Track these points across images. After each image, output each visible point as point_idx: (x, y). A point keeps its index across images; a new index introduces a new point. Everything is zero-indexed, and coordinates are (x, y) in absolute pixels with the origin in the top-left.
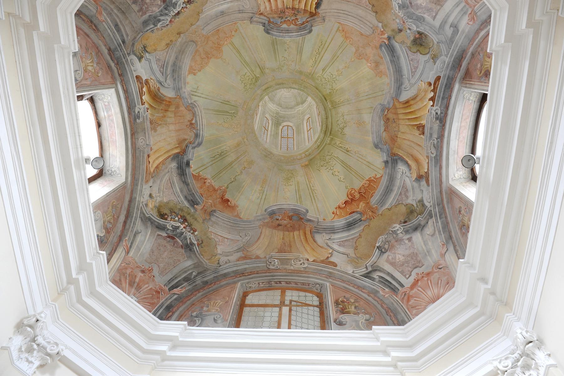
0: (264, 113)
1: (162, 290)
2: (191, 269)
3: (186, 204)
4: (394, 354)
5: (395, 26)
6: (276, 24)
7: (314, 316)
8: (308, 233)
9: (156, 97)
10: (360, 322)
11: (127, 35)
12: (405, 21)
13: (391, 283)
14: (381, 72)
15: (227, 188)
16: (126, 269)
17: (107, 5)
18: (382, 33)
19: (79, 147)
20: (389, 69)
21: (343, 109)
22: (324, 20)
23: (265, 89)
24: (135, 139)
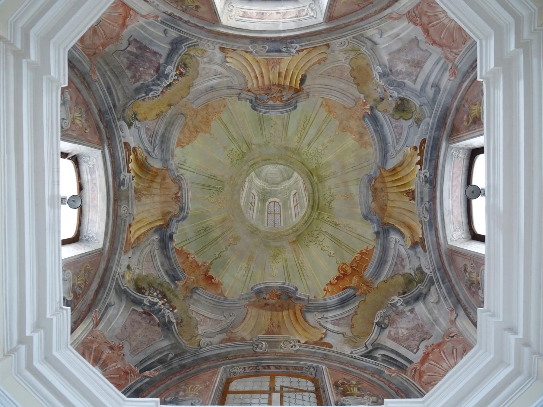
0: (250, 189)
1: (132, 371)
3: (167, 279)
5: (377, 96)
6: (263, 100)
8: (298, 312)
9: (143, 166)
11: (119, 100)
12: (387, 89)
13: (397, 361)
14: (366, 142)
15: (211, 264)
17: (101, 65)
18: (365, 104)
19: (56, 183)
20: (373, 139)
21: (329, 183)
22: (308, 95)
23: (252, 165)
24: (118, 206)
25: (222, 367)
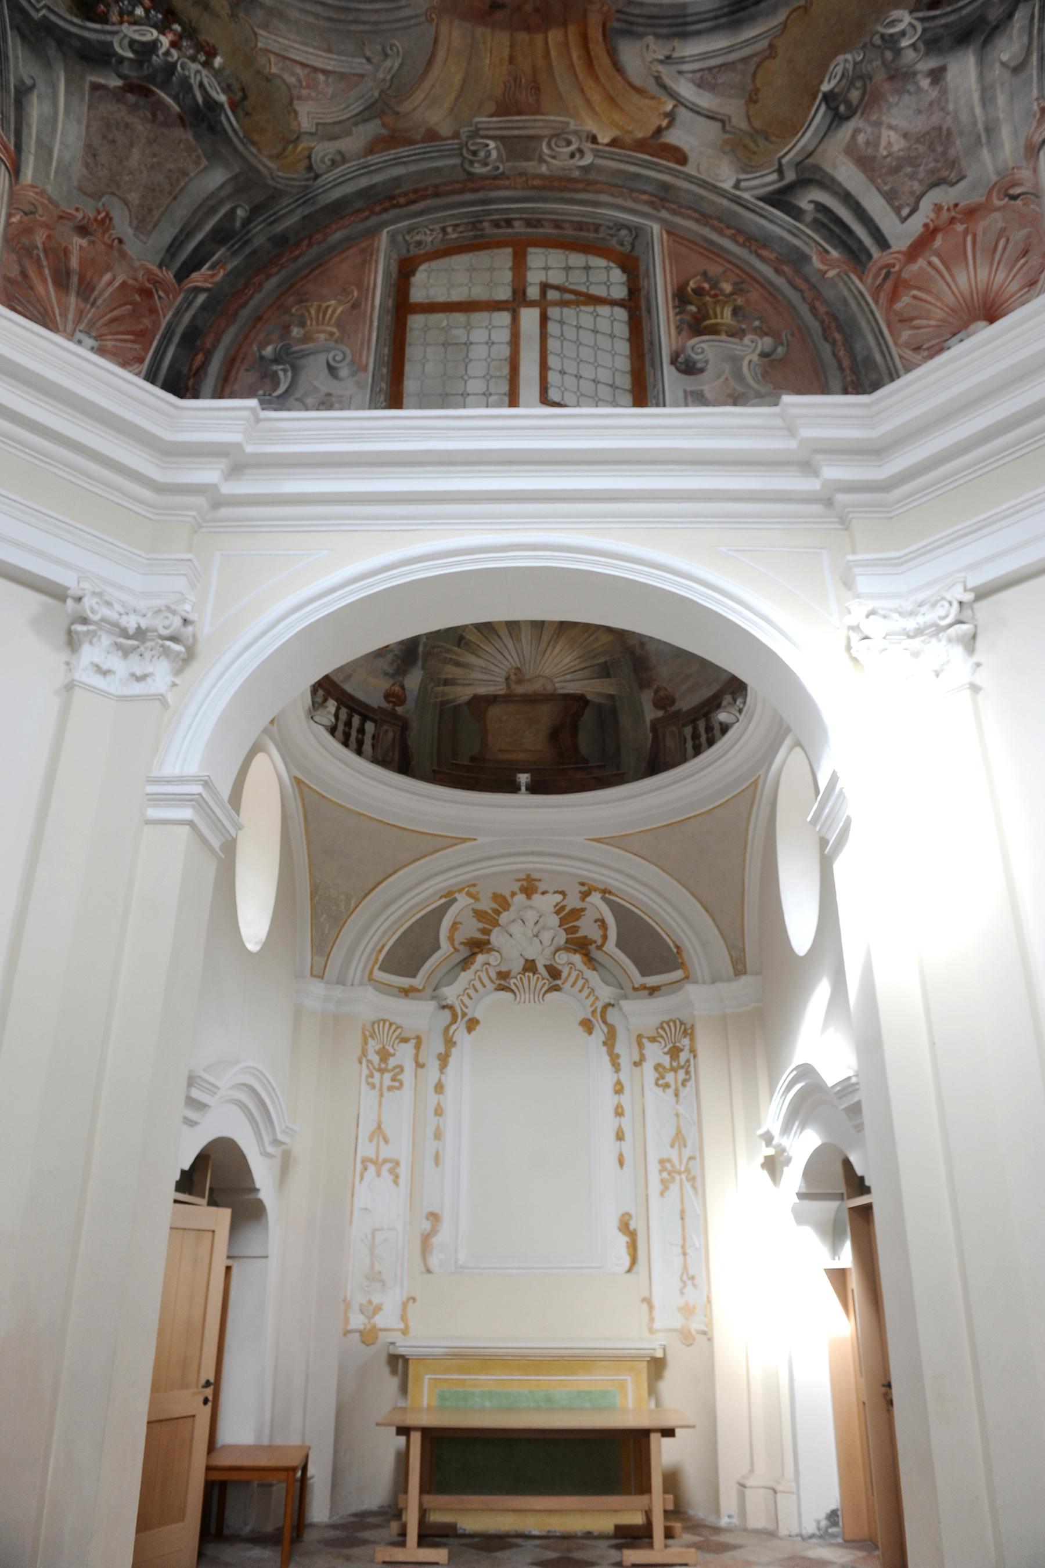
1: (156, 282)
2: (228, 197)
4: (833, 472)
7: (612, 336)
8: (595, 34)
10: (746, 362)
13: (849, 231)
16: (29, 230)
25: (385, 231)
